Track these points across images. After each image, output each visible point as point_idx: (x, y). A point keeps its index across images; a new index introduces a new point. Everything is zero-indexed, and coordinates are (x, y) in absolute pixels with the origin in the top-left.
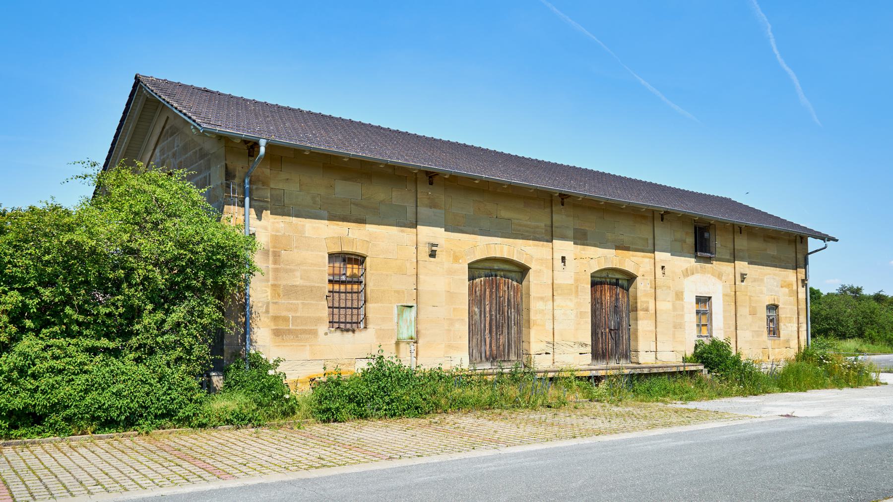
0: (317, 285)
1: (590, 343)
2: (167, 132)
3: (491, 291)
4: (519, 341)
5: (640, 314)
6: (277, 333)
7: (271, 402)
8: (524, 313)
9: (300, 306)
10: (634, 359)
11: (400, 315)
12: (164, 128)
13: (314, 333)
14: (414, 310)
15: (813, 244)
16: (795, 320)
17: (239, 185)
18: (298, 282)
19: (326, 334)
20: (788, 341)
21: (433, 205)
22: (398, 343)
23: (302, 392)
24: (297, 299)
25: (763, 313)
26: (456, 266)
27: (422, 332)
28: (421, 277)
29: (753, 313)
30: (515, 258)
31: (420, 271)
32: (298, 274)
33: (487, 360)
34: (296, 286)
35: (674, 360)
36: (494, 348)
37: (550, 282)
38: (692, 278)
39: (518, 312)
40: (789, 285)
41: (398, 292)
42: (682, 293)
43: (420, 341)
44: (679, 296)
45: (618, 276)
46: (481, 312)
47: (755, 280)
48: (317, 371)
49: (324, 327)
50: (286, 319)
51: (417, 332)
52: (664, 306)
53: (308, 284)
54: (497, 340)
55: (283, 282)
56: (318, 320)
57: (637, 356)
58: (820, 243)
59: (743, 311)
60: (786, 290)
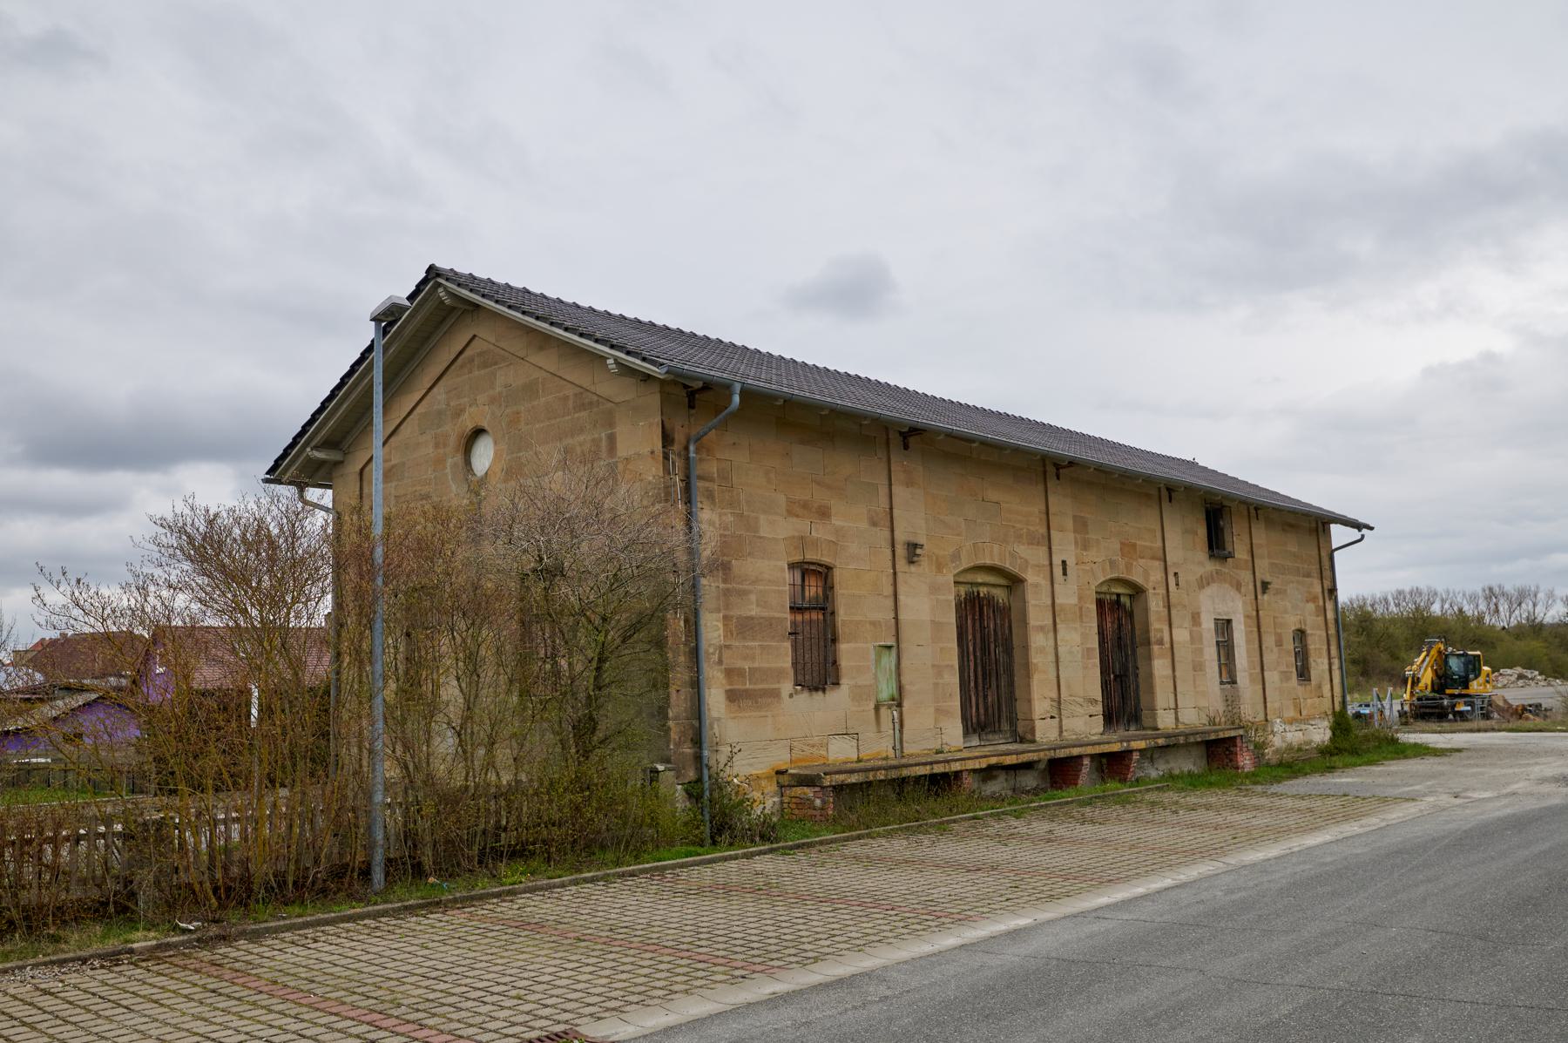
0: (777, 615)
1: (1100, 699)
2: (471, 360)
3: (974, 620)
4: (1012, 698)
5: (1155, 648)
6: (732, 696)
7: (719, 824)
8: (1017, 653)
9: (758, 651)
10: (1146, 722)
11: (878, 661)
12: (461, 353)
13: (775, 694)
14: (894, 651)
15: (1339, 534)
16: (1325, 653)
17: (679, 455)
18: (754, 611)
19: (791, 696)
20: (1319, 687)
21: (909, 483)
22: (877, 708)
23: (765, 802)
24: (754, 639)
25: (1289, 645)
26: (940, 579)
27: (907, 687)
28: (901, 598)
29: (1279, 643)
30: (1007, 565)
31: (901, 589)
32: (753, 597)
33: (975, 731)
34: (752, 618)
35: (1197, 723)
36: (982, 711)
37: (1049, 602)
38: (1208, 591)
39: (1009, 651)
40: (1314, 599)
41: (873, 623)
42: (1198, 614)
43: (906, 704)
44: (1196, 619)
45: (1120, 590)
46: (985, 649)
47: (1278, 592)
48: (780, 757)
49: (787, 686)
50: (740, 673)
51: (900, 688)
52: (1181, 635)
53: (765, 614)
54: (985, 697)
55: (735, 612)
56: (779, 674)
57: (1154, 717)
58: (1354, 534)
59: (1269, 641)
60: (1311, 606)
